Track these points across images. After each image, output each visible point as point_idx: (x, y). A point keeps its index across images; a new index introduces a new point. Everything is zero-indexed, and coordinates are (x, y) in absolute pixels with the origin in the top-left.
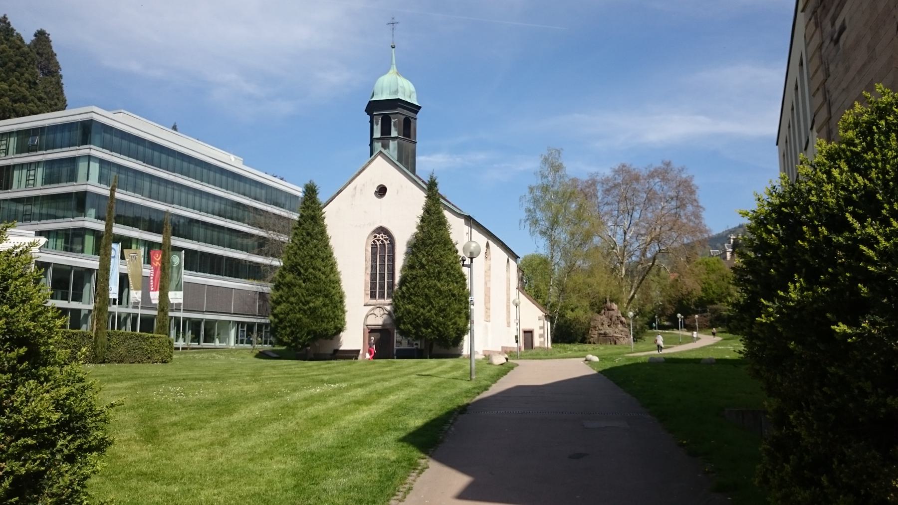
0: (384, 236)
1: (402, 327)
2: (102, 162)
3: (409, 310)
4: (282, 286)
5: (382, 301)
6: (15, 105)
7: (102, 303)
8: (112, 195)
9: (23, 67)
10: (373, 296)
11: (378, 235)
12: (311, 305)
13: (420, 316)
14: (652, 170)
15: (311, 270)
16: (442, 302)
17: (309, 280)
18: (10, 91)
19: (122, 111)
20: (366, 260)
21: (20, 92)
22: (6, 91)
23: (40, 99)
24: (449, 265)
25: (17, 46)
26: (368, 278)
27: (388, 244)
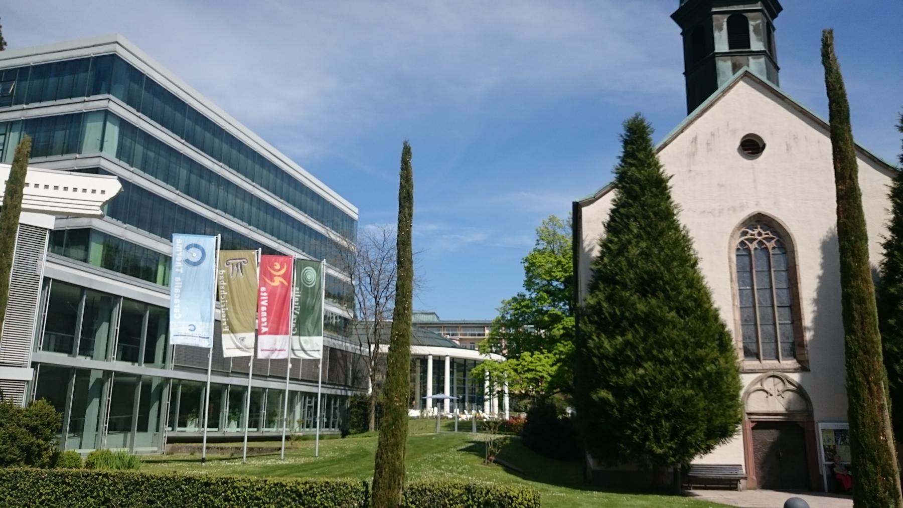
2: (124, 125)
11: (750, 232)
20: (732, 281)
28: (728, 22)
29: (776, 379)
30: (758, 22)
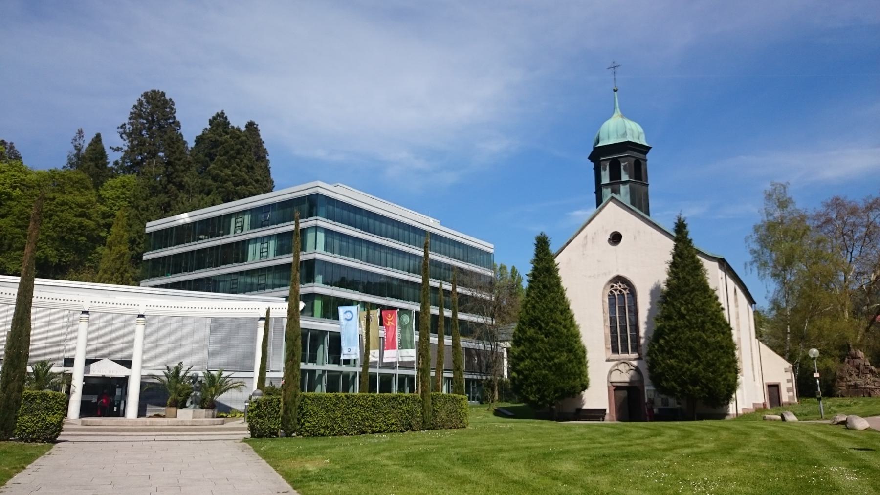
0: (622, 285)
1: (664, 384)
2: (327, 231)
3: (672, 365)
4: (522, 341)
5: (625, 356)
6: (237, 188)
7: (425, 363)
8: (426, 254)
9: (242, 154)
10: (615, 350)
11: (615, 285)
12: (556, 361)
13: (686, 372)
14: (871, 201)
15: (551, 324)
16: (710, 356)
17: (551, 334)
18: (233, 176)
19: (339, 184)
20: (604, 312)
21: (241, 176)
22: (229, 176)
23: (257, 181)
24: (713, 313)
25: (237, 136)
26: (608, 331)
27: (628, 294)
29: (626, 364)
30: (626, 163)
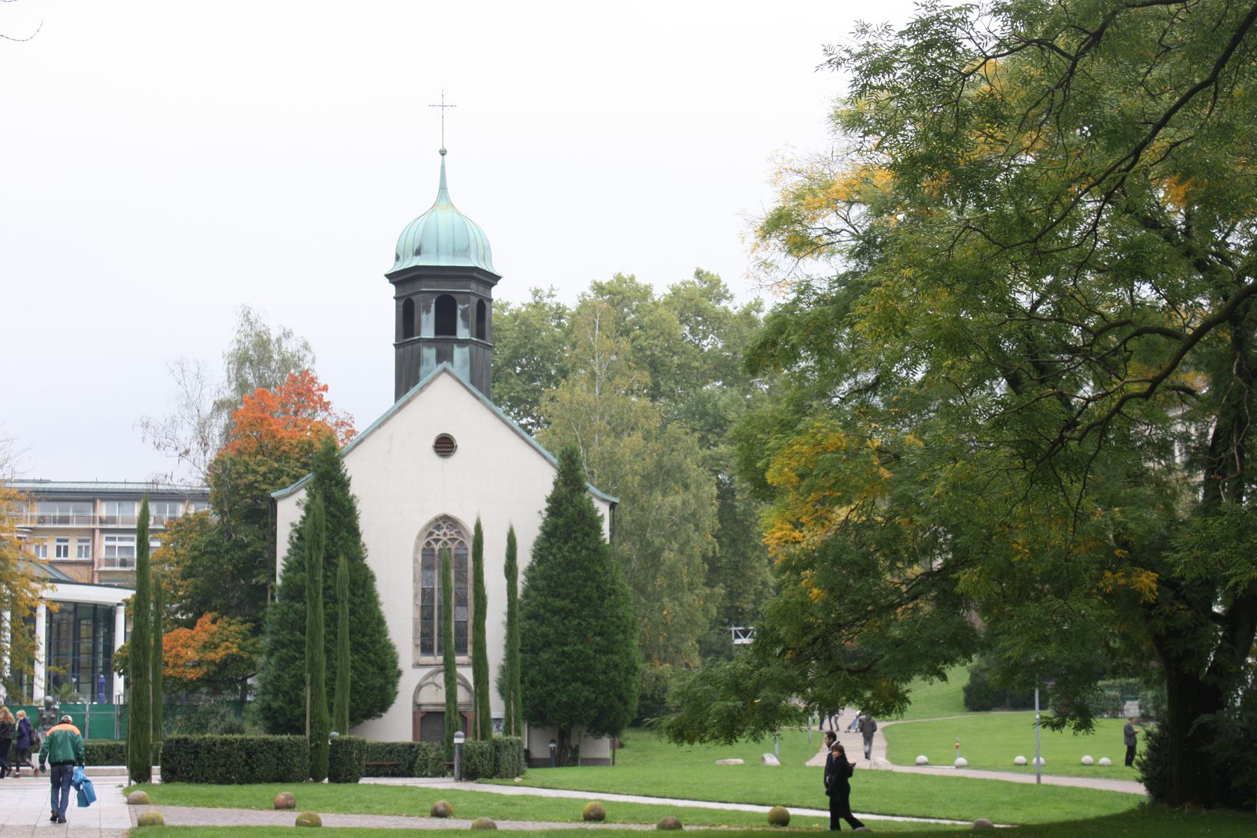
11: (436, 532)
28: (436, 303)
